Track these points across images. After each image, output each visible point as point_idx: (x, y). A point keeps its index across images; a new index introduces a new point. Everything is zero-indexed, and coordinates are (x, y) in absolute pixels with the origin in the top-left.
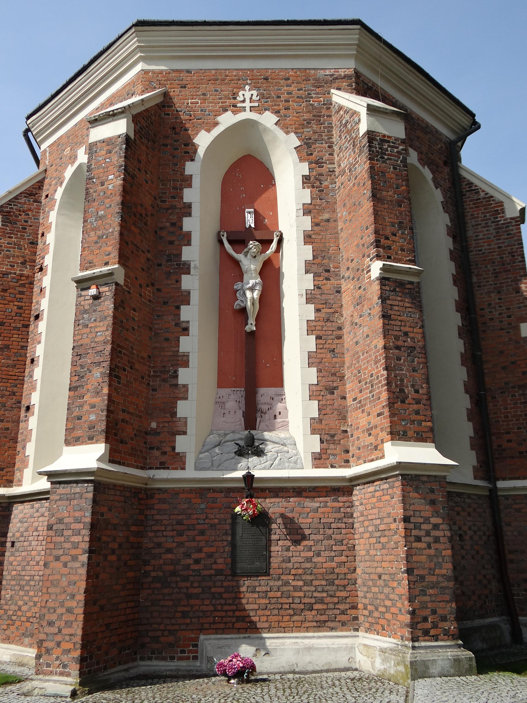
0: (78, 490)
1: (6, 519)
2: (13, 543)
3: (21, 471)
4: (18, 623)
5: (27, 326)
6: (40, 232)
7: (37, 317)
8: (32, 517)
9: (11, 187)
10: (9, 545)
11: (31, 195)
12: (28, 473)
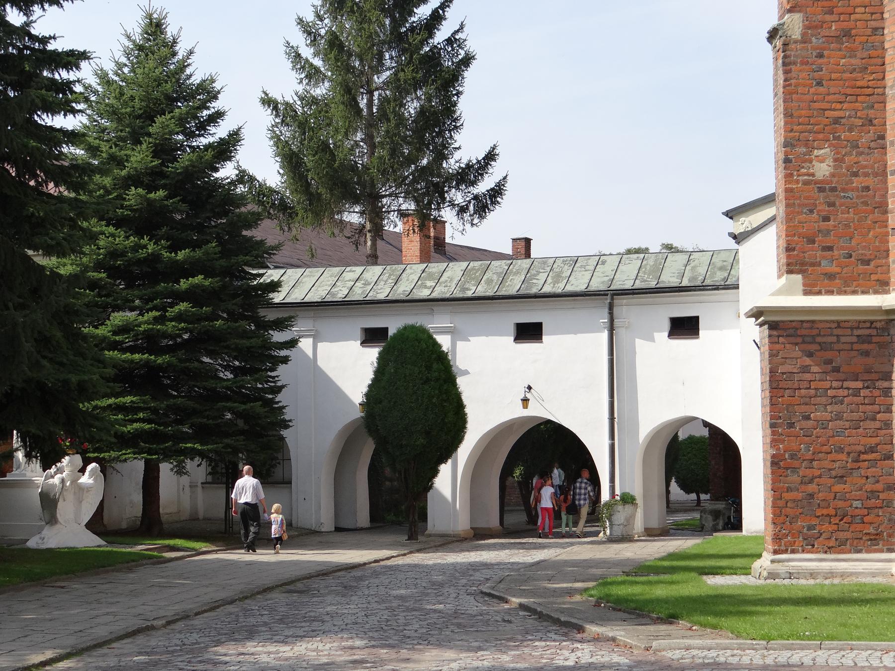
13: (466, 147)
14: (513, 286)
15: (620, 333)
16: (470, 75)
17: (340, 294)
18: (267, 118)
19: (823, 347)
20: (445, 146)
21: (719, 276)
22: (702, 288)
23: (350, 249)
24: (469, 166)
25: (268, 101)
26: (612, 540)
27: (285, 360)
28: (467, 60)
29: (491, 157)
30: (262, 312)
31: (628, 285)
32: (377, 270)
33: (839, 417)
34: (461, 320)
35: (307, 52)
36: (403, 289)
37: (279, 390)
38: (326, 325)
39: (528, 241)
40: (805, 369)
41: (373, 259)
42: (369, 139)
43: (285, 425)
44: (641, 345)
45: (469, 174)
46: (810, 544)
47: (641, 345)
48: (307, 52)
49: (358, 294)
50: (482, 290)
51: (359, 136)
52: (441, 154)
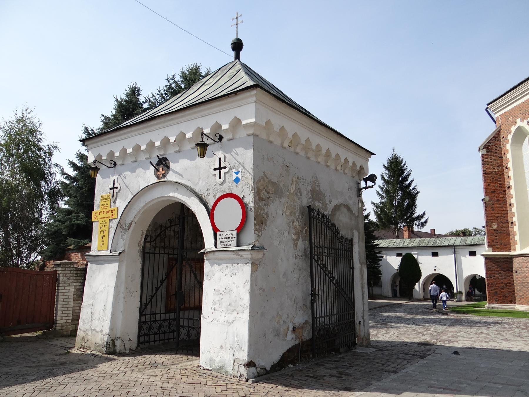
0: (499, 387)
1: (512, 263)
2: (516, 272)
3: (514, 246)
4: (525, 298)
5: (505, 191)
6: (503, 153)
7: (509, 187)
8: (523, 262)
9: (487, 137)
10: (514, 272)
11: (496, 138)
12: (518, 247)
13: (418, 212)
14: (431, 244)
15: (457, 255)
16: (419, 197)
17: (391, 245)
18: (373, 207)
19: (497, 262)
20: (413, 211)
21: (481, 242)
22: (476, 245)
23: (391, 234)
24: (419, 216)
25: (373, 203)
26: (457, 301)
27: (381, 260)
28: (418, 193)
29: (424, 213)
30: (375, 250)
31: (458, 244)
32: (399, 240)
33: (501, 276)
34: (419, 251)
35: (381, 193)
36: (405, 244)
37: (380, 266)
38: (388, 252)
39: (434, 230)
40: (493, 266)
41: (398, 237)
42: (395, 211)
43: (381, 274)
44: (463, 258)
45: (419, 218)
46: (496, 302)
47: (463, 258)
48: (381, 193)
49: (395, 246)
50: (423, 245)
51: (393, 210)
52: (412, 214)
